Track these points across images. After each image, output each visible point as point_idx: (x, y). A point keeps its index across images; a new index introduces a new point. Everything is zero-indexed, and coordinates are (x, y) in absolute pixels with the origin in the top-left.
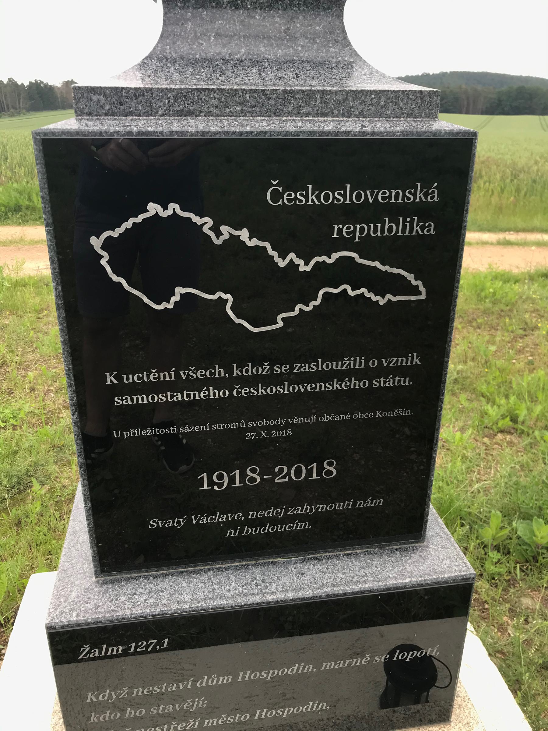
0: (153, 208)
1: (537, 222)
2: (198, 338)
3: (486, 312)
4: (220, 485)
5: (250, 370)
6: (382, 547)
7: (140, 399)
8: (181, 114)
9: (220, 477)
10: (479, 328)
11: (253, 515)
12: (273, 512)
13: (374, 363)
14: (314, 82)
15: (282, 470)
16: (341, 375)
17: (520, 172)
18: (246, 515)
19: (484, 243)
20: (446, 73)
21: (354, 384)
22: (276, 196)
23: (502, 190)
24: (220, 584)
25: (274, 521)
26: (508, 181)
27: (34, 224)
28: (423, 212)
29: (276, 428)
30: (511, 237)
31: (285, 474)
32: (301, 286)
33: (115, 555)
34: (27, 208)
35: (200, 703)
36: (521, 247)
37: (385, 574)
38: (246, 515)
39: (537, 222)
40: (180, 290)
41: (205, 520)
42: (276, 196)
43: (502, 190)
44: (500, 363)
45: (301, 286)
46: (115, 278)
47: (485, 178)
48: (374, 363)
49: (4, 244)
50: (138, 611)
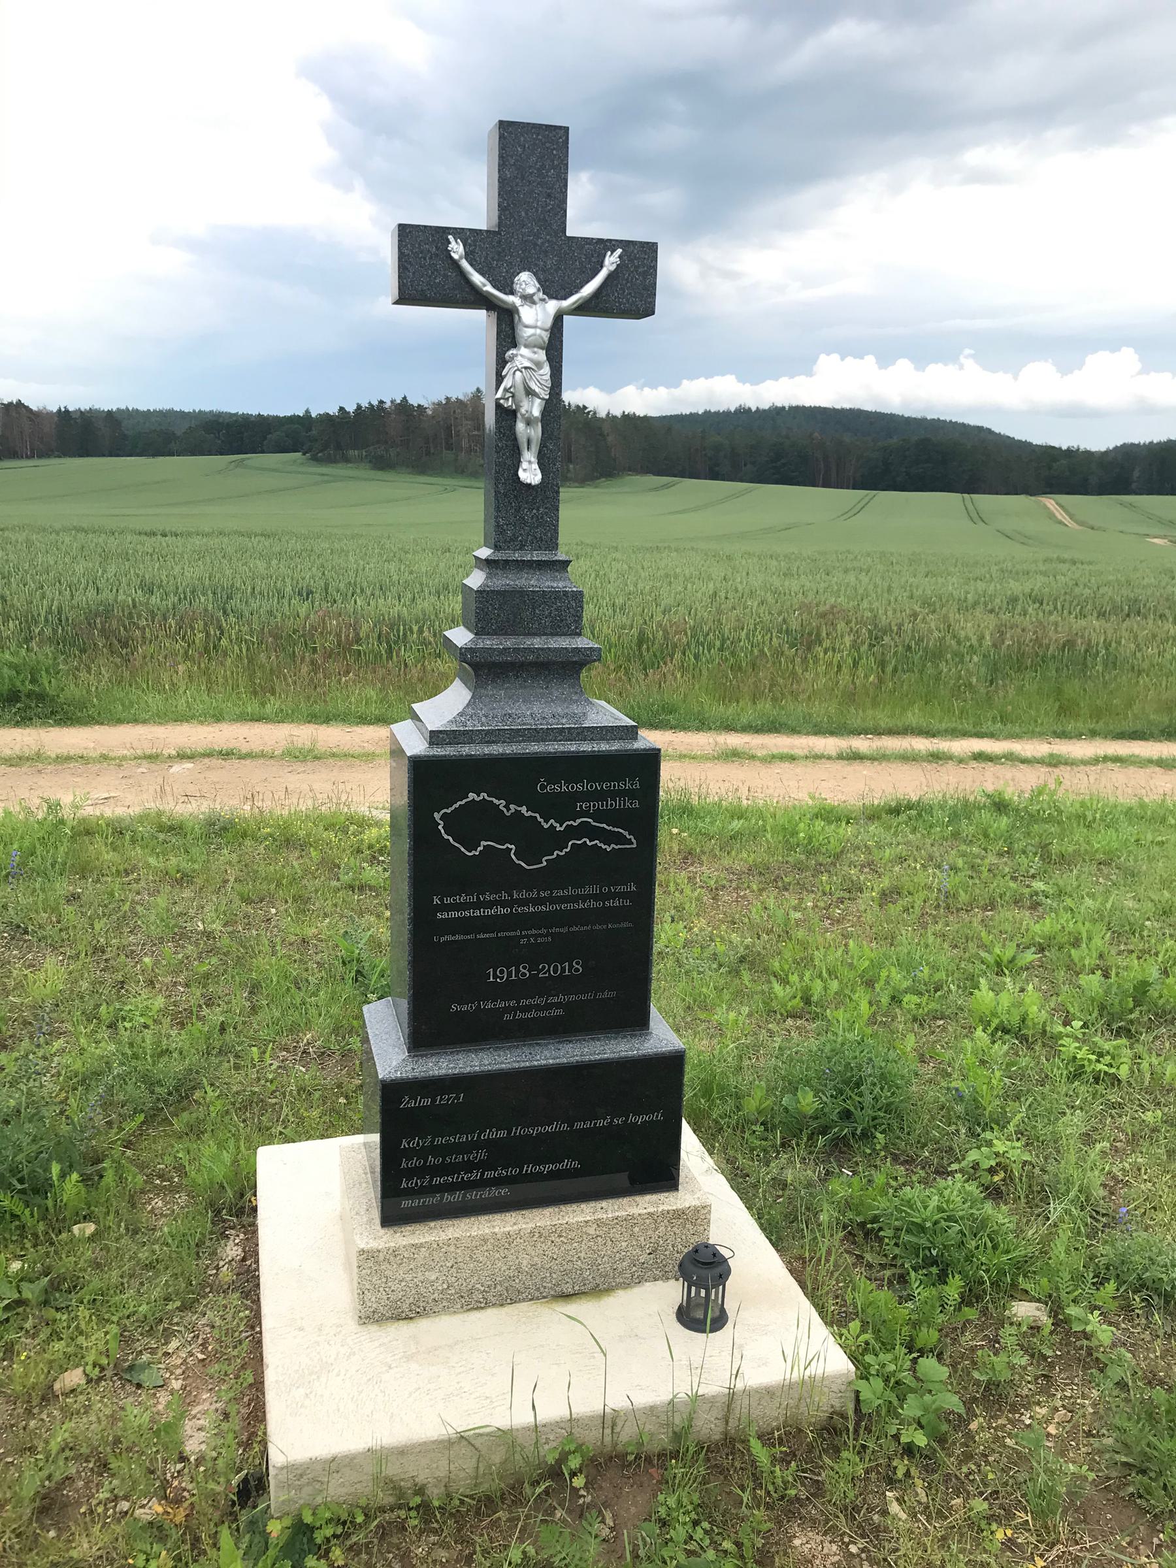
0: (472, 796)
1: (913, 717)
2: (493, 874)
3: (800, 867)
4: (501, 978)
5: (524, 894)
6: (617, 1033)
7: (454, 914)
8: (489, 742)
9: (502, 972)
10: (787, 890)
11: (523, 1002)
12: (537, 1001)
13: (605, 890)
14: (564, 721)
15: (544, 967)
16: (584, 898)
17: (885, 633)
18: (518, 1003)
19: (817, 757)
20: (784, 408)
21: (593, 904)
22: (543, 787)
23: (856, 663)
24: (499, 1056)
25: (538, 1008)
26: (864, 648)
27: (44, 724)
28: (631, 794)
29: (541, 935)
30: (861, 744)
31: (547, 971)
32: (559, 840)
33: (423, 1036)
34: (29, 695)
35: (482, 1155)
36: (876, 763)
37: (619, 1049)
38: (518, 1003)
39: (913, 717)
40: (483, 843)
41: (490, 1006)
42: (543, 787)
43: (856, 663)
44: (801, 934)
45: (559, 840)
46: (446, 837)
47: (827, 643)
48: (605, 890)
49: (16, 761)
50: (443, 1072)
